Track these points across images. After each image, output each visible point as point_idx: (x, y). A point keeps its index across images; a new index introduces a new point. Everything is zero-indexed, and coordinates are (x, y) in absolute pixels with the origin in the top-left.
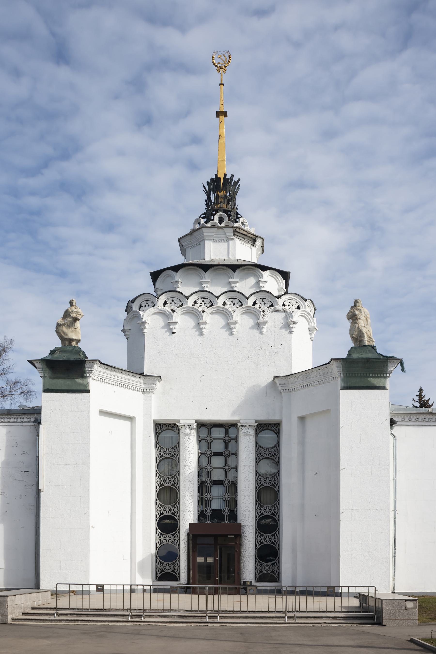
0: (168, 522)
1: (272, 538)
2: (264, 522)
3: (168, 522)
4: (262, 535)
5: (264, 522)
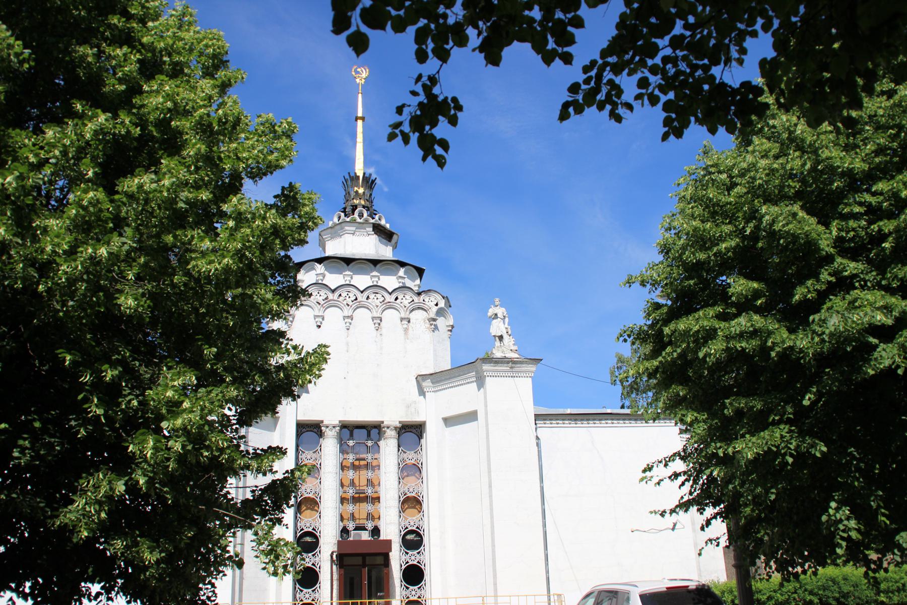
0: (308, 539)
1: (418, 556)
2: (409, 537)
3: (308, 539)
4: (408, 588)
5: (409, 537)
